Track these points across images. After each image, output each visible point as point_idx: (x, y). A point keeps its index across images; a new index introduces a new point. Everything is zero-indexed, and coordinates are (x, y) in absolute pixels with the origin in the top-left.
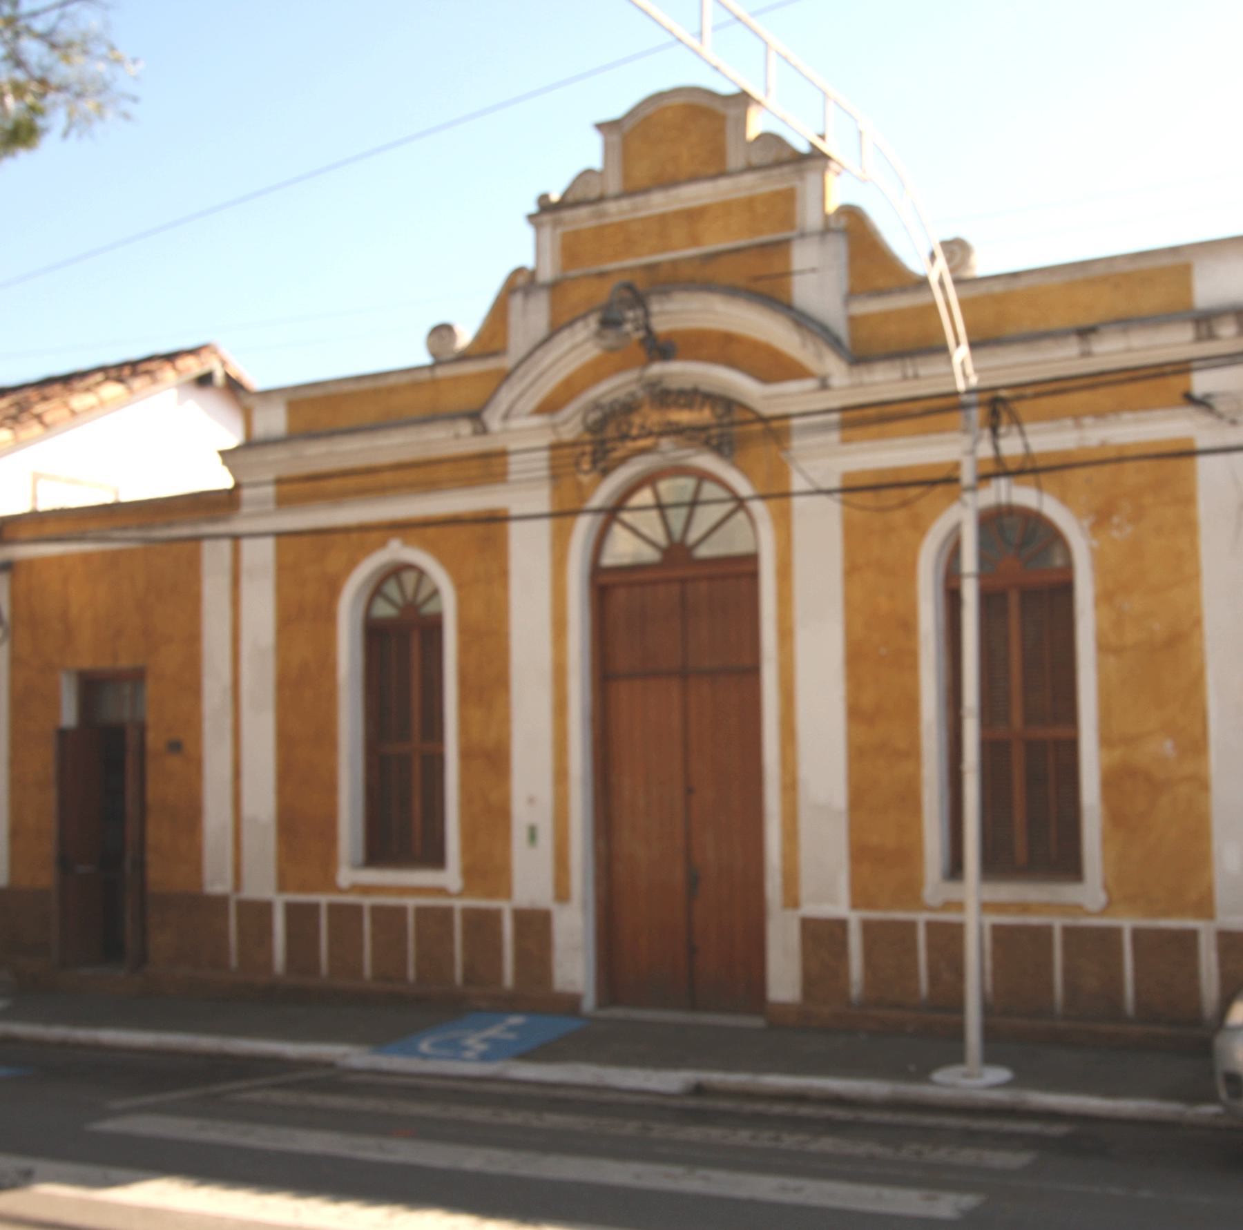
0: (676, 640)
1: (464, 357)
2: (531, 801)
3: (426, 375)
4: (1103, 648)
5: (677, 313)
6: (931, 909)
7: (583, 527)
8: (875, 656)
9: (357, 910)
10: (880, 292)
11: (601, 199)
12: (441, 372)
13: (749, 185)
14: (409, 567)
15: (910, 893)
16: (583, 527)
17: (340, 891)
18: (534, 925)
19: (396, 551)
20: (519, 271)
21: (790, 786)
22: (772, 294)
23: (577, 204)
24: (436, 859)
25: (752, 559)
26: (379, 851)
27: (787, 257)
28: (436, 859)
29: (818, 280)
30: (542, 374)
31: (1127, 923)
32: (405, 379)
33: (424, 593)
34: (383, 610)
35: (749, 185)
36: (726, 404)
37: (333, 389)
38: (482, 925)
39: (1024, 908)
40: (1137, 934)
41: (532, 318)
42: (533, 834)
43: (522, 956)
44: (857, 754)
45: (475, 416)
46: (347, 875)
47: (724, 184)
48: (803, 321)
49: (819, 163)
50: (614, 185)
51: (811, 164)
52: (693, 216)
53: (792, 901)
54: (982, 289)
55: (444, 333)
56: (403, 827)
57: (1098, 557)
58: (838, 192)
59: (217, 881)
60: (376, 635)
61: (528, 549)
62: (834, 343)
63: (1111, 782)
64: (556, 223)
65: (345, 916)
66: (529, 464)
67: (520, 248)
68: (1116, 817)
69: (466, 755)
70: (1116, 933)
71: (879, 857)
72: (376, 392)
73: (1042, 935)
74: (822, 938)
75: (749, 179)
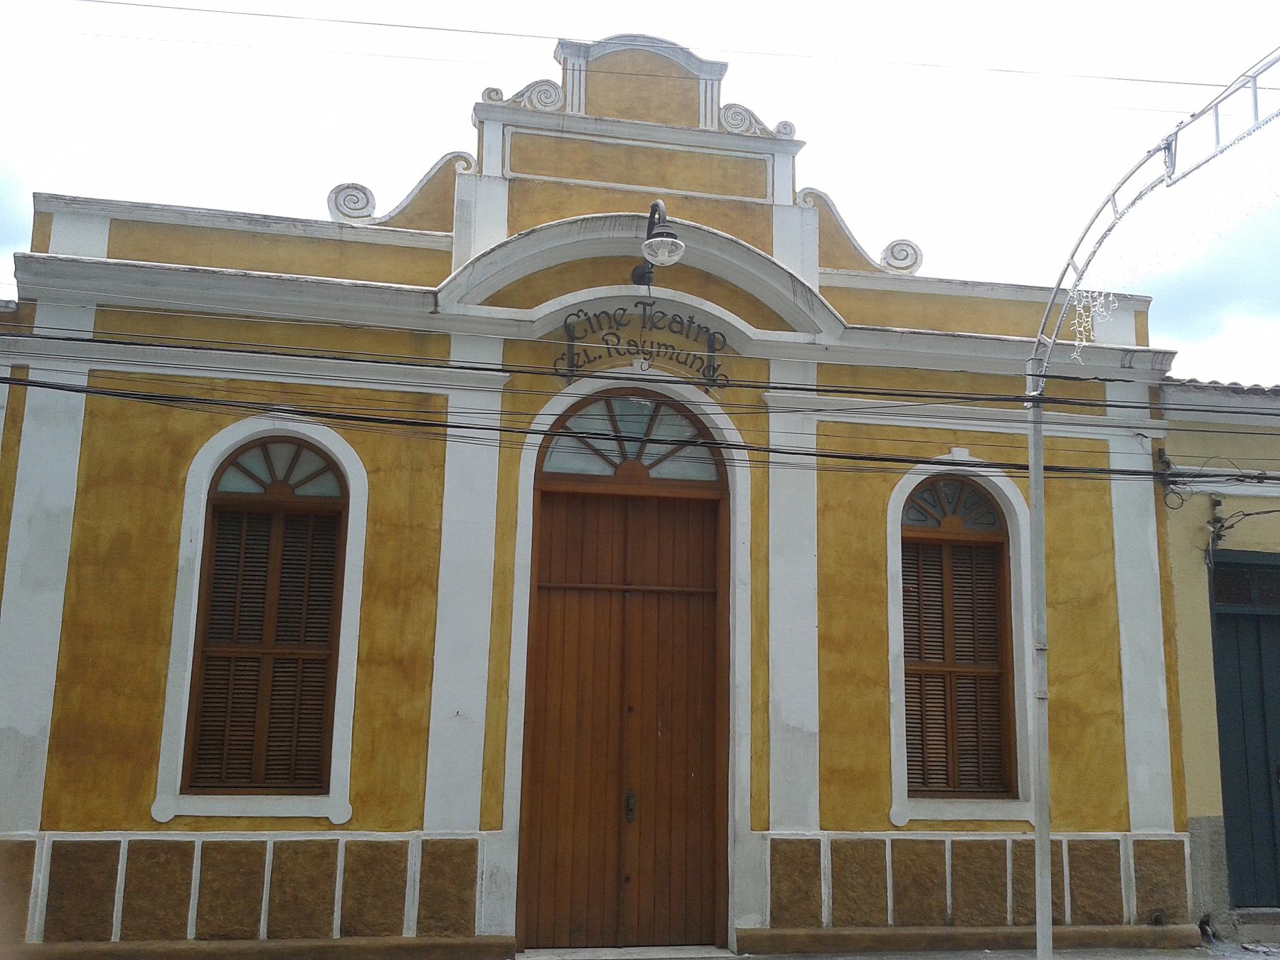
6: (897, 828)
8: (842, 591)
9: (184, 850)
17: (158, 826)
18: (452, 864)
21: (761, 707)
24: (318, 783)
28: (318, 783)
32: (299, 232)
34: (236, 484)
36: (714, 339)
39: (980, 824)
44: (828, 680)
46: (168, 800)
58: (809, 171)
65: (161, 862)
68: (1057, 746)
69: (365, 661)
71: (846, 783)
74: (793, 861)
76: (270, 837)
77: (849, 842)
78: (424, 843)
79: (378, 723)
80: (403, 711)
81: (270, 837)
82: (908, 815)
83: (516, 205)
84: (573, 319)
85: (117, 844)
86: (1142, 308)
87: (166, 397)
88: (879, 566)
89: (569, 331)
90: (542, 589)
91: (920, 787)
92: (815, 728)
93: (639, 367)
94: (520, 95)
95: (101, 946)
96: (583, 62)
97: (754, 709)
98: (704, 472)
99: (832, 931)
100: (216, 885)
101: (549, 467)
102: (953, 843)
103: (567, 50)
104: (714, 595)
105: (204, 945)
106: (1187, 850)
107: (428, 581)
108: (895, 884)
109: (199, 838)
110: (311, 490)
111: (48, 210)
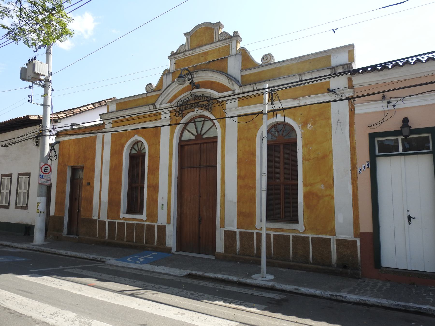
0: (198, 157)
1: (153, 91)
2: (163, 198)
3: (145, 96)
4: (304, 159)
5: (199, 77)
6: (258, 230)
7: (179, 128)
8: (246, 162)
10: (249, 69)
11: (185, 51)
12: (148, 95)
13: (219, 45)
14: (140, 141)
15: (252, 224)
16: (179, 128)
18: (162, 229)
19: (137, 138)
20: (166, 70)
21: (223, 196)
22: (223, 72)
23: (180, 53)
24: (142, 213)
25: (216, 137)
26: (130, 210)
28: (142, 213)
29: (234, 66)
30: (169, 94)
31: (310, 236)
32: (141, 97)
33: (142, 148)
34: (134, 152)
35: (219, 45)
36: (211, 99)
39: (282, 230)
40: (312, 238)
41: (169, 79)
42: (162, 207)
44: (240, 188)
45: (154, 104)
46: (122, 216)
47: (213, 45)
48: (229, 76)
49: (235, 38)
50: (188, 48)
51: (233, 38)
52: (206, 54)
53: (223, 226)
56: (134, 206)
57: (303, 134)
59: (95, 216)
60: (132, 157)
62: (237, 82)
63: (306, 196)
64: (175, 58)
66: (166, 118)
67: (166, 64)
68: (307, 206)
69: (149, 187)
71: (246, 215)
72: (135, 100)
73: (287, 238)
74: (230, 236)
75: (219, 43)
76: (135, 222)
80: (154, 197)
86: (351, 49)
92: (235, 200)
96: (189, 37)
99: (126, 243)
102: (274, 235)
106: (359, 244)
107: (158, 169)
109: (126, 222)
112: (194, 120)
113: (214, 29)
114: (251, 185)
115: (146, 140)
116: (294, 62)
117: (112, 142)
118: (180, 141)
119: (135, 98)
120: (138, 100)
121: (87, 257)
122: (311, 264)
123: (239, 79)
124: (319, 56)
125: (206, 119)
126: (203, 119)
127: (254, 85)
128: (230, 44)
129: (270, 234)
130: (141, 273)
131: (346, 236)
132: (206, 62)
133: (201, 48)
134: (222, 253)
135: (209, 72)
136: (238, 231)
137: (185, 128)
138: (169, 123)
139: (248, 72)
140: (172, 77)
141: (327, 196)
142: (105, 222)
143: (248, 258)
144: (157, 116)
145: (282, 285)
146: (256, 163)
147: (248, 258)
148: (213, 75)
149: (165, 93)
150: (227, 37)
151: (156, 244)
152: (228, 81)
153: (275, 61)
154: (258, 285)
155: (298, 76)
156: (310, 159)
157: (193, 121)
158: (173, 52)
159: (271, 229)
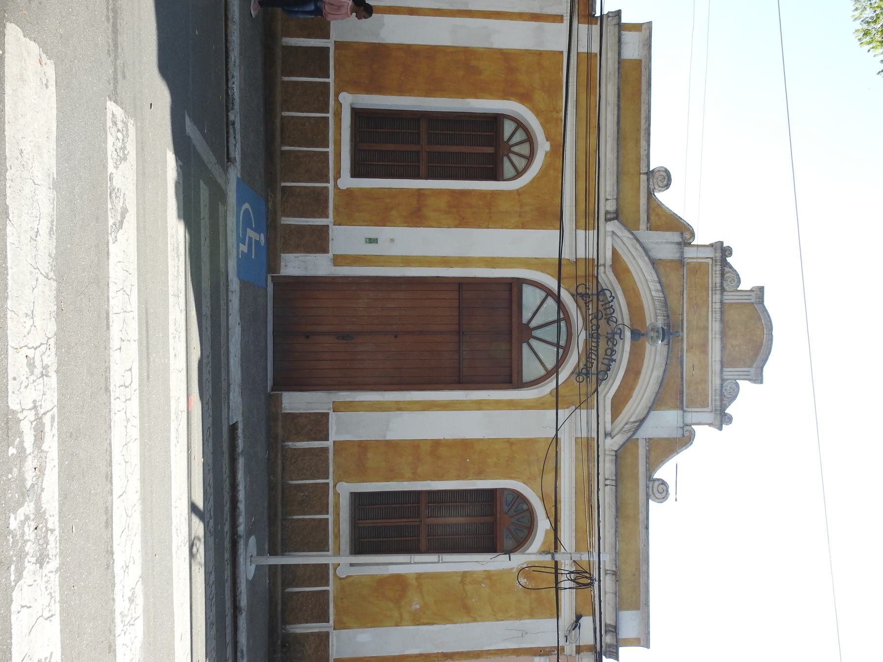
1: (650, 195)
2: (392, 240)
5: (655, 354)
6: (335, 486)
7: (552, 283)
8: (464, 454)
9: (326, 109)
11: (723, 290)
16: (552, 283)
17: (337, 95)
18: (317, 241)
19: (543, 147)
20: (693, 235)
21: (399, 407)
22: (657, 403)
23: (723, 275)
24: (356, 173)
27: (675, 407)
28: (356, 173)
31: (331, 588)
32: (643, 153)
34: (508, 127)
36: (603, 375)
37: (644, 97)
38: (317, 203)
39: (337, 536)
40: (327, 592)
41: (663, 245)
42: (372, 241)
43: (300, 230)
44: (415, 445)
46: (348, 100)
47: (717, 367)
50: (729, 298)
52: (704, 348)
54: (642, 509)
55: (665, 183)
58: (703, 433)
61: (540, 243)
65: (319, 98)
66: (579, 244)
69: (420, 193)
70: (327, 584)
71: (359, 454)
74: (317, 425)
75: (717, 382)
77: (327, 458)
78: (327, 226)
79: (388, 201)
81: (331, 150)
82: (342, 491)
83: (669, 264)
84: (608, 294)
85: (328, 77)
86: (642, 642)
87: (553, 89)
88: (480, 474)
89: (600, 292)
90: (461, 284)
91: (358, 499)
92: (391, 436)
93: (583, 336)
94: (731, 267)
95: (279, 71)
96: (753, 301)
97: (397, 402)
98: (527, 376)
100: (307, 124)
101: (527, 290)
102: (327, 520)
103: (760, 291)
104: (459, 383)
105: (278, 121)
107: (462, 222)
108: (305, 485)
109: (330, 115)
110: (507, 164)
111: (644, 30)
112: (564, 319)
113: (751, 366)
114: (419, 470)
115: (532, 182)
116: (641, 545)
117: (540, 53)
118: (519, 283)
119: (642, 133)
120: (638, 141)
121: (231, 65)
122: (283, 590)
123: (635, 437)
124: (642, 589)
125: (561, 351)
126: (562, 343)
127: (614, 483)
128: (709, 409)
129: (328, 513)
130: (223, 331)
131: (335, 648)
132: (687, 329)
133: (718, 336)
134: (281, 408)
135: (661, 374)
136: (329, 444)
137: (549, 292)
138: (566, 255)
139: (642, 452)
140: (671, 261)
141: (401, 615)
142: (327, 36)
143: (279, 469)
144: (589, 218)
145: (245, 626)
146: (463, 479)
147: (279, 469)
148: (652, 381)
149: (636, 249)
150: (728, 395)
151: (283, 184)
152: (632, 420)
153: (650, 501)
154: (238, 581)
155: (614, 569)
156: (464, 584)
157: (562, 316)
158: (731, 254)
159: (338, 515)
